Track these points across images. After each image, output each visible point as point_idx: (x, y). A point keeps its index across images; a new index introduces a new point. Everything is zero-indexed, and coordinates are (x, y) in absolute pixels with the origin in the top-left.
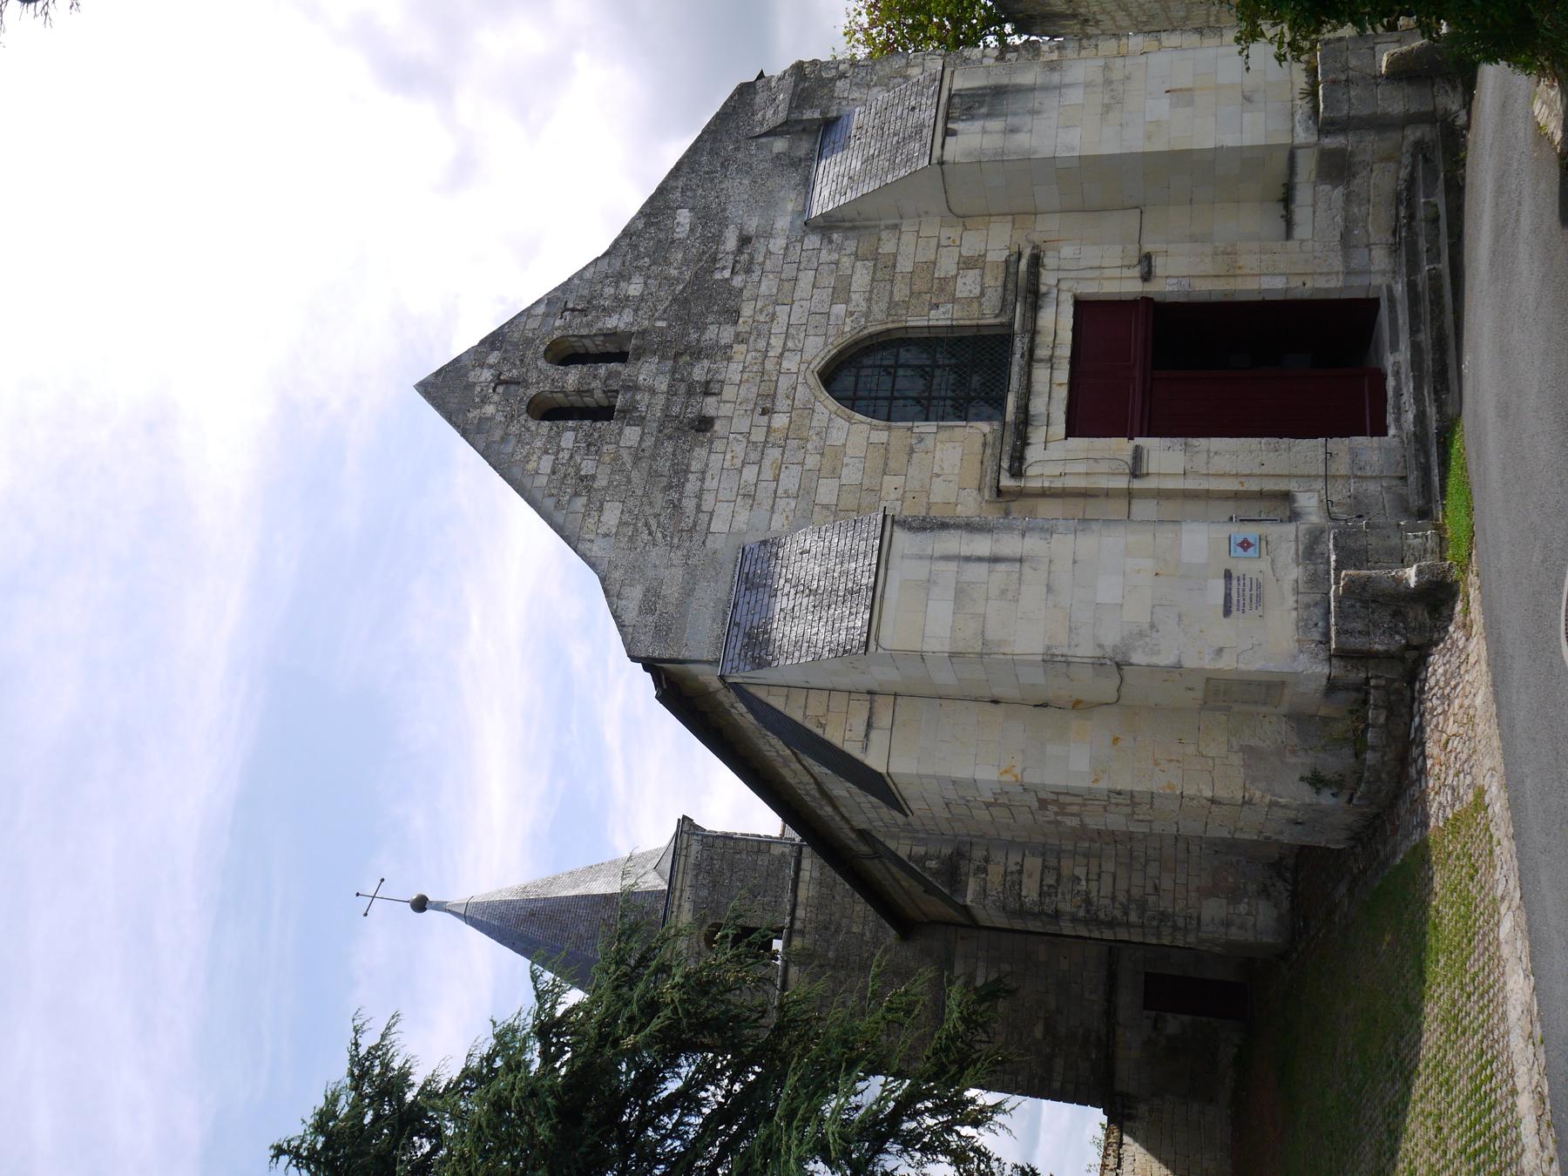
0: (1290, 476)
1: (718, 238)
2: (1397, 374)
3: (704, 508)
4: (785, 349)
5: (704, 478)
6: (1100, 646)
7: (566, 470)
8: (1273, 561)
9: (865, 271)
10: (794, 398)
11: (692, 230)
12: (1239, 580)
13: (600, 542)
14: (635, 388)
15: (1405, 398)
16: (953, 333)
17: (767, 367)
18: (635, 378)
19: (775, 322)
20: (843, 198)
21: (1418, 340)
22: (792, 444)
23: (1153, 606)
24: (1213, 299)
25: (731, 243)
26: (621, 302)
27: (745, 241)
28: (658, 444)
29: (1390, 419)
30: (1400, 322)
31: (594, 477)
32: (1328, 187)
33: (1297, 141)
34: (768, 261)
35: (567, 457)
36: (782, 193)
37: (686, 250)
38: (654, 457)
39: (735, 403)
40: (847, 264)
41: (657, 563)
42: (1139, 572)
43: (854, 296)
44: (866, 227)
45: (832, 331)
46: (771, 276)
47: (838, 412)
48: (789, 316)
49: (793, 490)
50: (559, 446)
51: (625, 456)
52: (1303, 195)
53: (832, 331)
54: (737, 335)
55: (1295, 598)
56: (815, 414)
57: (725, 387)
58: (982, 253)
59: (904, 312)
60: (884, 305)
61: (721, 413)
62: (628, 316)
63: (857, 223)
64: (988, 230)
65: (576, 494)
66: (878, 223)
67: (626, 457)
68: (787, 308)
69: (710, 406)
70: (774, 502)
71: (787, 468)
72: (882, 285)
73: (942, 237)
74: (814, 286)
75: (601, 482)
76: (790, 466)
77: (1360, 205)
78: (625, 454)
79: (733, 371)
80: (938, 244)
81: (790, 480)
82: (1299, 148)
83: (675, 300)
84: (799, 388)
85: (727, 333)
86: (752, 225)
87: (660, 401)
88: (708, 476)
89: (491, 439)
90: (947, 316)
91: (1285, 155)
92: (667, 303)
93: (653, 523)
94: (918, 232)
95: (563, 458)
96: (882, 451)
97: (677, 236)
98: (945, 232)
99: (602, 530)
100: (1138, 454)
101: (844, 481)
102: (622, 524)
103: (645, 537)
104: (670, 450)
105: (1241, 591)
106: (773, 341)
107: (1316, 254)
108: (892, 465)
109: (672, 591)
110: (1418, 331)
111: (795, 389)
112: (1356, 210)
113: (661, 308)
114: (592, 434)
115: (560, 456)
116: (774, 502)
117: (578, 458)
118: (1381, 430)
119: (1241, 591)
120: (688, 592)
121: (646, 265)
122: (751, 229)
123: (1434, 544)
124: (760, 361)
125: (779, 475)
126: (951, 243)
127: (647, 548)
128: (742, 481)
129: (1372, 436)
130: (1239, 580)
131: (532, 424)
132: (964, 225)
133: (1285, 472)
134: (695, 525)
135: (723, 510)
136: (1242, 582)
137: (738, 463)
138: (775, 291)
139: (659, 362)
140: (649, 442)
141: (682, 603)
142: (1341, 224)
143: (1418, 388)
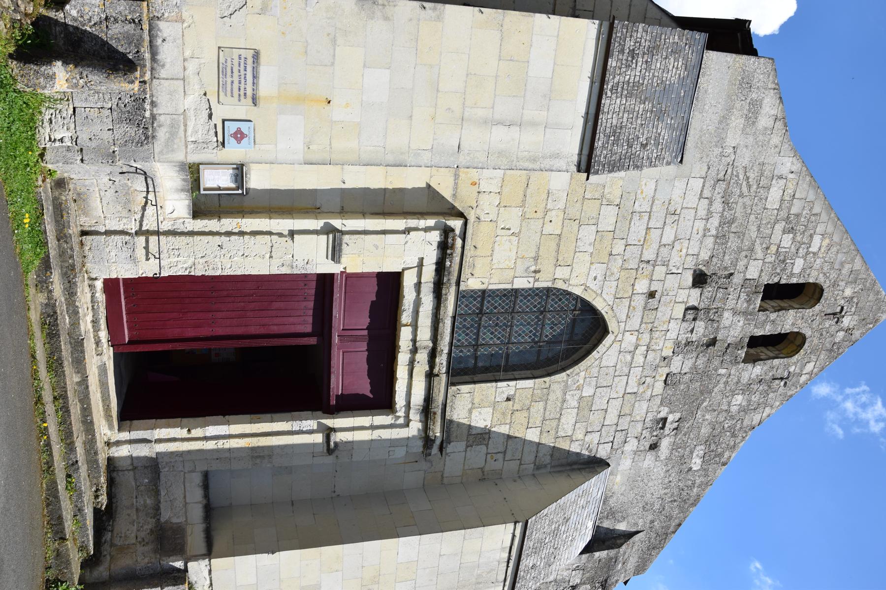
0: (192, 233)
1: (674, 447)
2: (98, 343)
3: (706, 202)
4: (633, 353)
5: (705, 230)
6: (386, 19)
7: (803, 238)
8: (210, 116)
9: (565, 426)
10: (629, 307)
11: (692, 452)
12: (245, 94)
13: (784, 170)
14: (745, 313)
15: (89, 318)
16: (494, 376)
17: (648, 336)
18: (746, 322)
19: (638, 377)
20: (585, 488)
21: (79, 375)
22: (633, 264)
23: (333, 64)
24: (269, 416)
25: (665, 444)
26: (747, 389)
27: (654, 447)
28: (734, 264)
29: (101, 297)
30: (99, 395)
31: (784, 232)
32: (175, 520)
33: (204, 563)
34: (640, 430)
35: (801, 250)
36: (623, 489)
37: (698, 437)
38: (740, 250)
39: (675, 302)
40: (578, 432)
41: (745, 150)
42: (347, 105)
43: (575, 404)
44: (562, 465)
45: (594, 371)
46: (638, 418)
47: (594, 295)
48: (627, 383)
49: (636, 217)
50: (805, 260)
51: (760, 251)
52: (197, 513)
53: (594, 371)
54: (668, 365)
55: (187, 73)
56: (614, 293)
57: (681, 316)
58: (469, 448)
59: (535, 391)
60: (552, 397)
61: (687, 291)
62: (745, 378)
63: (568, 468)
64: (463, 470)
65: (798, 216)
66: (552, 470)
67: (759, 254)
68: (628, 391)
69: (694, 297)
70: (651, 209)
71: (639, 241)
72: (552, 416)
73: (501, 460)
74: (606, 411)
75: (779, 227)
76: (636, 243)
77: (145, 506)
78: (759, 254)
79: (676, 330)
80: (505, 455)
81: (638, 229)
82: (204, 555)
83: (710, 393)
84: (624, 318)
85: (676, 365)
86: (649, 459)
87: (731, 303)
88: (701, 233)
89: (850, 266)
90: (501, 390)
91: (216, 548)
92: (716, 390)
93: (745, 189)
94: (521, 464)
95: (804, 249)
96: (560, 259)
97: (703, 447)
98: (498, 465)
99: (782, 182)
100: (335, 253)
101: (594, 228)
102: (768, 188)
103: (751, 175)
104: (727, 257)
105: (243, 81)
106: (642, 359)
107: (181, 459)
108: (553, 245)
109: (737, 121)
110: (79, 384)
111: (628, 316)
112: (149, 501)
113: (721, 385)
114: (781, 270)
115: (805, 250)
116: (651, 209)
117: (793, 250)
118: (111, 286)
119: (243, 81)
120: (724, 120)
121: (727, 421)
122: (650, 457)
123: (42, 131)
124: (653, 341)
125: (646, 233)
126: (495, 457)
127: (751, 165)
128: (675, 227)
129: (117, 280)
130: (245, 94)
131: (821, 280)
132: (483, 472)
133: (197, 238)
134: (715, 185)
135: (692, 200)
136: (242, 93)
137: (677, 246)
138: (637, 405)
139: (727, 337)
140: (741, 264)
141: (730, 109)
142: (161, 488)
143: (75, 324)
